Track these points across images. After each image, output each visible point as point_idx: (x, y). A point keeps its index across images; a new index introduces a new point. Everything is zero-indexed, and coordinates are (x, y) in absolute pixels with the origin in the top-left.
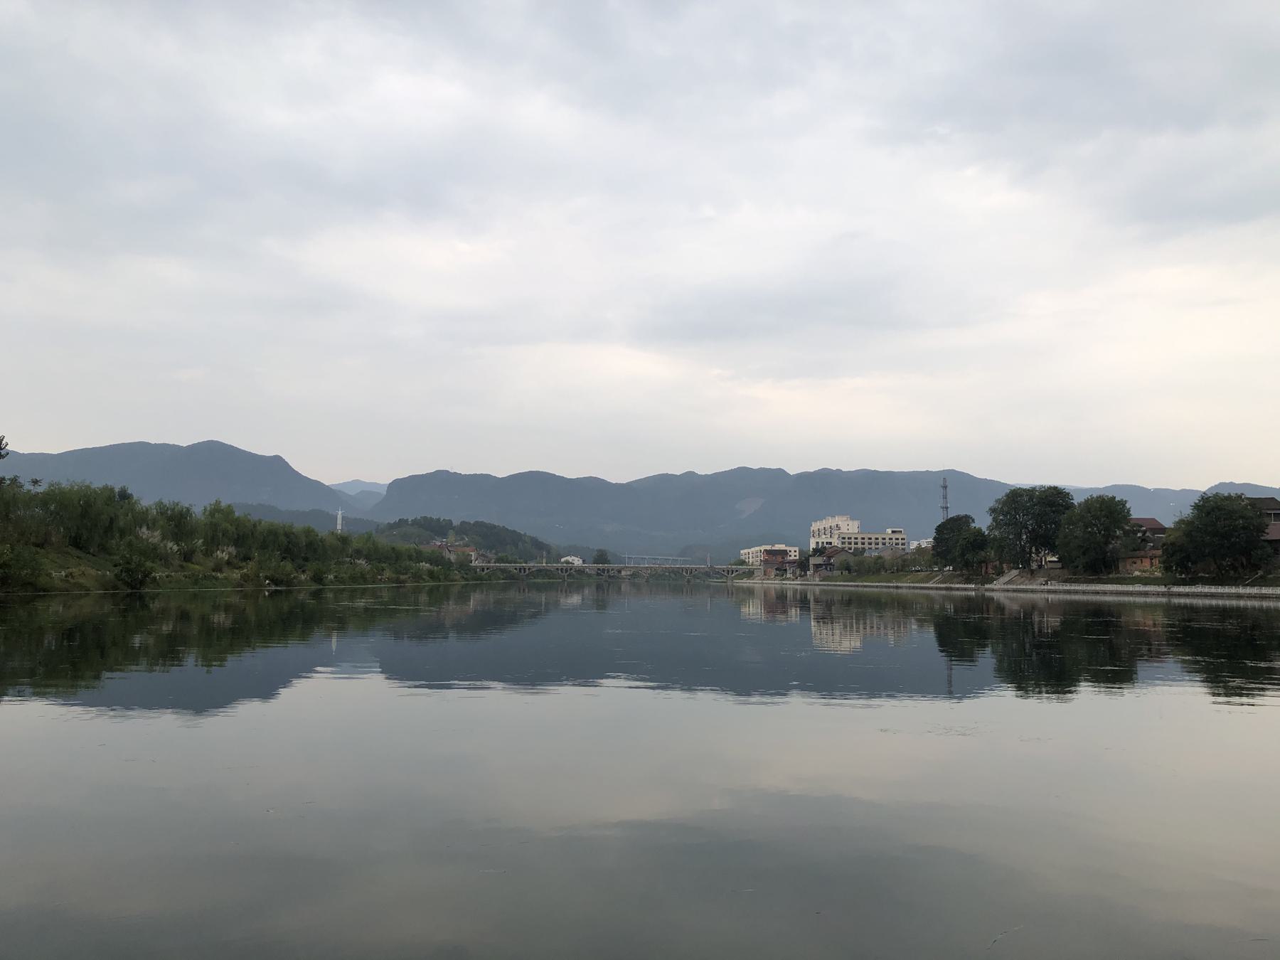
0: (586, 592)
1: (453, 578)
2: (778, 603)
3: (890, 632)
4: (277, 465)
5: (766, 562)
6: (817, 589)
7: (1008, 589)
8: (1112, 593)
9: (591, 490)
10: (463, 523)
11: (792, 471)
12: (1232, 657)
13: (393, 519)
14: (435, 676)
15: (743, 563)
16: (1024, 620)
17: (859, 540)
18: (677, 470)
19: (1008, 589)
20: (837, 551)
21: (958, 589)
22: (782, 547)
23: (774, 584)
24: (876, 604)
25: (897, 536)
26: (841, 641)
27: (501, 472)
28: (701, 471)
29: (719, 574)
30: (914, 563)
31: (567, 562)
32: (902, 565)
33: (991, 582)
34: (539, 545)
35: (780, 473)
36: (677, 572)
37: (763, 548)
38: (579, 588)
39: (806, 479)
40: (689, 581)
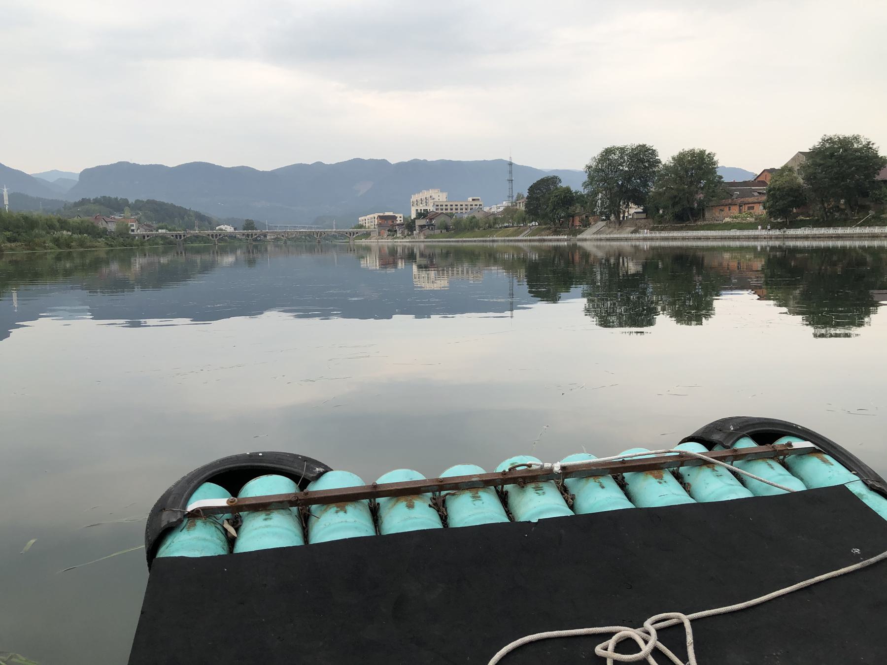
0: (239, 252)
2: (389, 259)
3: (471, 276)
5: (379, 225)
6: (422, 245)
7: (594, 239)
8: (715, 238)
9: (242, 177)
10: (137, 201)
11: (393, 161)
12: (829, 294)
13: (78, 199)
15: (361, 227)
16: (612, 265)
17: (449, 207)
19: (594, 239)
20: (436, 215)
21: (550, 240)
22: (391, 214)
23: (387, 242)
24: (471, 256)
25: (476, 203)
26: (433, 282)
27: (171, 163)
28: (327, 162)
29: (343, 235)
30: (503, 220)
31: (221, 230)
32: (491, 224)
33: (581, 232)
34: (201, 218)
35: (383, 163)
36: (310, 235)
37: (376, 215)
38: (233, 251)
39: (401, 166)
40: (319, 242)
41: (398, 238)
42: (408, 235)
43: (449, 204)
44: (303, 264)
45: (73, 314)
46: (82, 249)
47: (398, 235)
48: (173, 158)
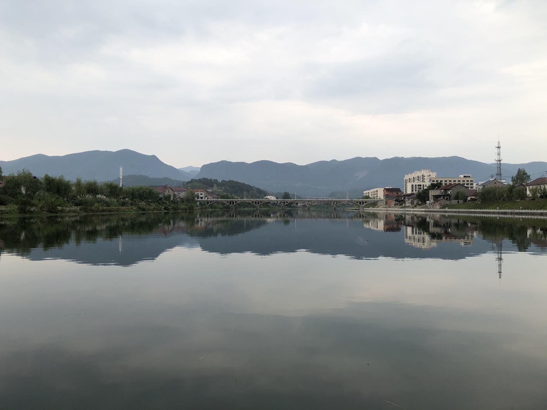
1: (232, 208)
4: (154, 158)
6: (438, 215)
11: (381, 158)
14: (224, 250)
15: (368, 197)
18: (328, 158)
23: (395, 210)
25: (468, 179)
27: (249, 161)
35: (375, 159)
39: (387, 162)
41: (408, 207)
42: (418, 204)
43: (444, 180)
44: (322, 225)
45: (192, 245)
46: (289, 209)
47: (407, 204)
48: (249, 156)
